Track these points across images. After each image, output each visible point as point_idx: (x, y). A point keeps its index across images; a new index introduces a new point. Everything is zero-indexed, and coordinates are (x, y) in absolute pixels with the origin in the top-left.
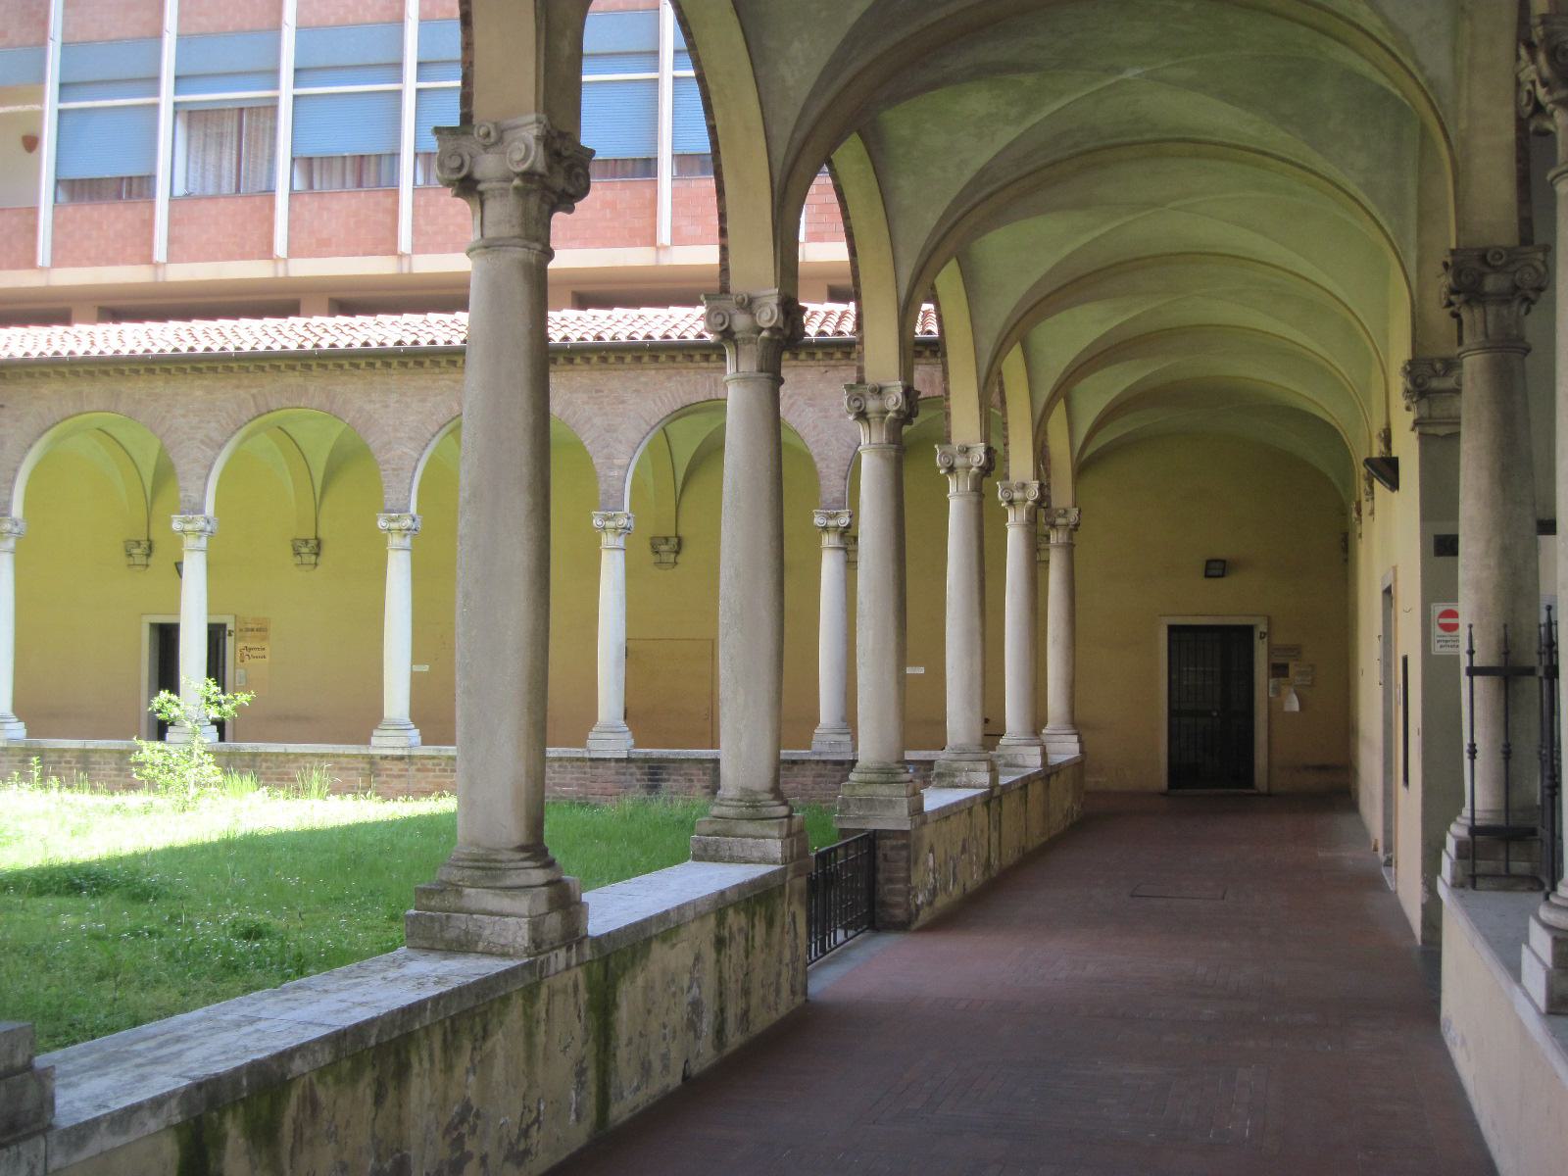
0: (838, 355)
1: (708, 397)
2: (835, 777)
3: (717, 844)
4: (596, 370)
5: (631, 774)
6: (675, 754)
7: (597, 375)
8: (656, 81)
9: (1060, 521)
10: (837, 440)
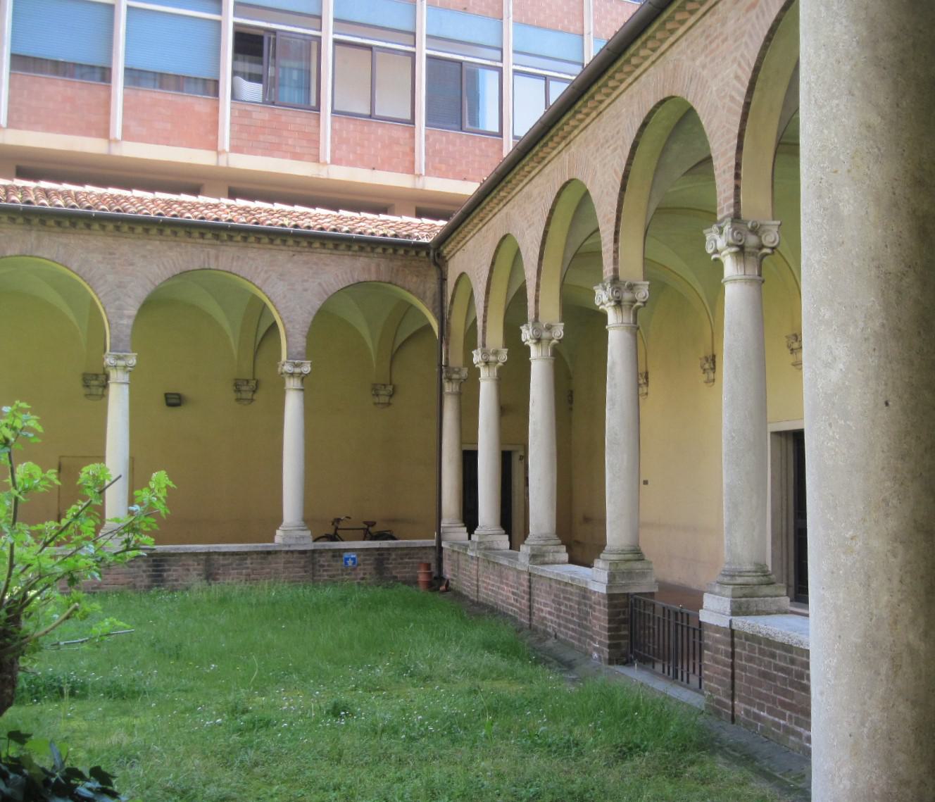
0: (305, 244)
1: (202, 267)
2: (300, 563)
3: (748, 603)
4: (110, 236)
5: (139, 567)
6: (175, 549)
7: (110, 240)
8: (219, 22)
9: (455, 376)
10: (301, 308)
